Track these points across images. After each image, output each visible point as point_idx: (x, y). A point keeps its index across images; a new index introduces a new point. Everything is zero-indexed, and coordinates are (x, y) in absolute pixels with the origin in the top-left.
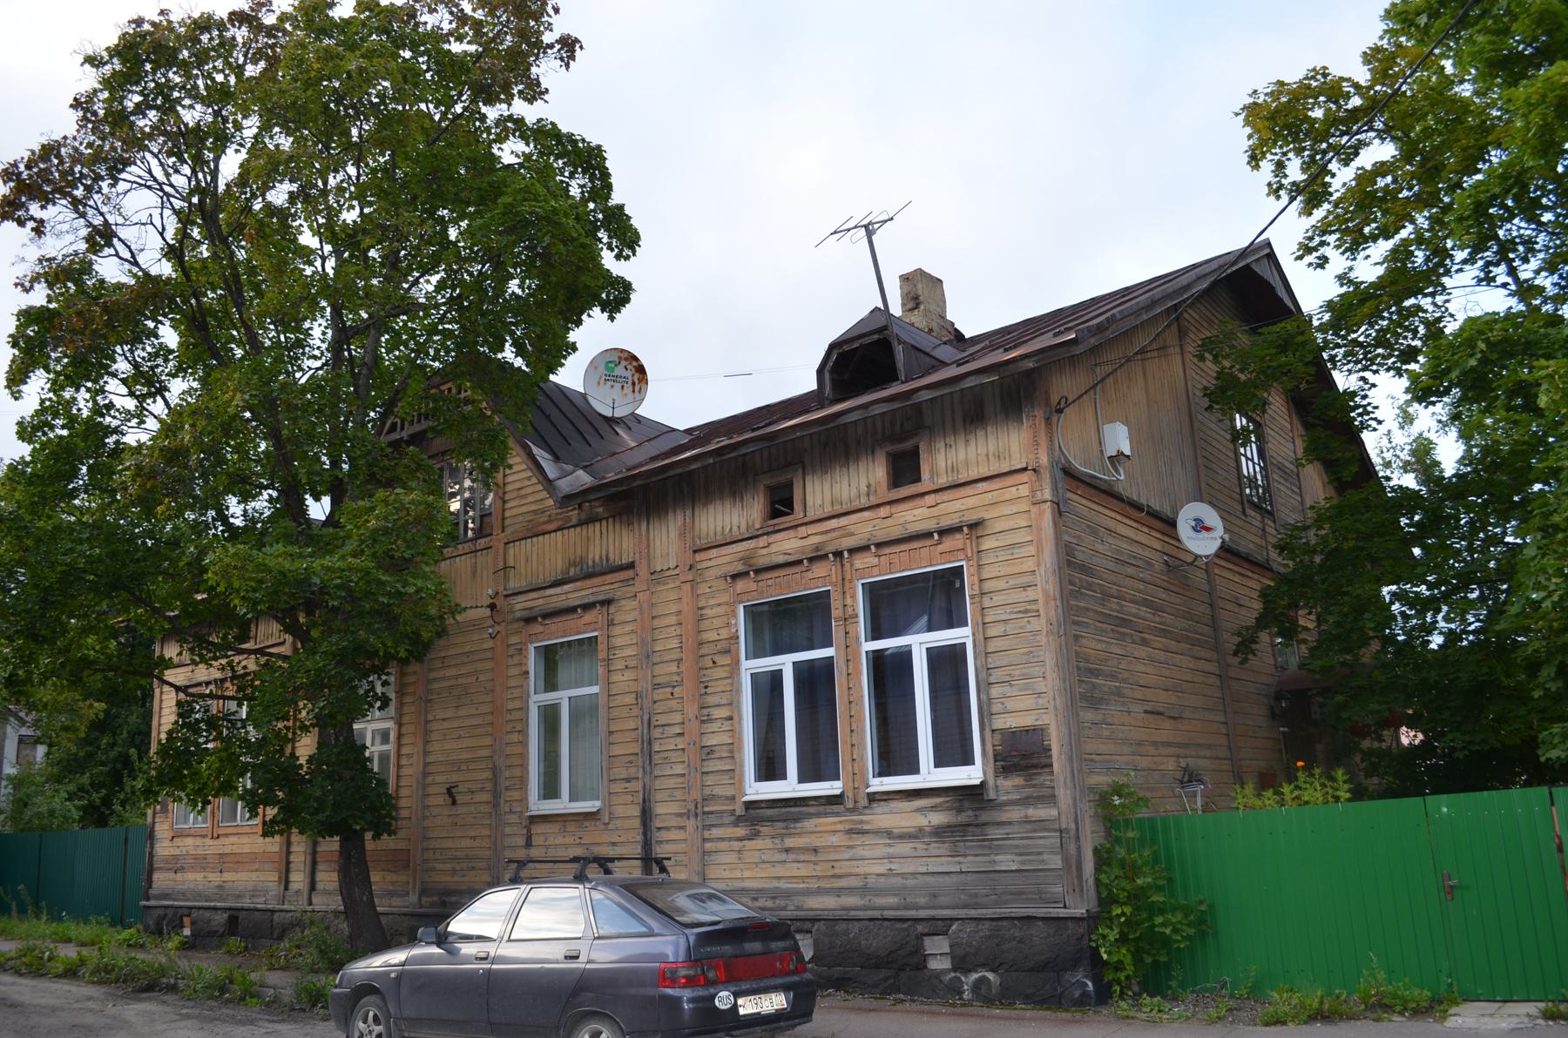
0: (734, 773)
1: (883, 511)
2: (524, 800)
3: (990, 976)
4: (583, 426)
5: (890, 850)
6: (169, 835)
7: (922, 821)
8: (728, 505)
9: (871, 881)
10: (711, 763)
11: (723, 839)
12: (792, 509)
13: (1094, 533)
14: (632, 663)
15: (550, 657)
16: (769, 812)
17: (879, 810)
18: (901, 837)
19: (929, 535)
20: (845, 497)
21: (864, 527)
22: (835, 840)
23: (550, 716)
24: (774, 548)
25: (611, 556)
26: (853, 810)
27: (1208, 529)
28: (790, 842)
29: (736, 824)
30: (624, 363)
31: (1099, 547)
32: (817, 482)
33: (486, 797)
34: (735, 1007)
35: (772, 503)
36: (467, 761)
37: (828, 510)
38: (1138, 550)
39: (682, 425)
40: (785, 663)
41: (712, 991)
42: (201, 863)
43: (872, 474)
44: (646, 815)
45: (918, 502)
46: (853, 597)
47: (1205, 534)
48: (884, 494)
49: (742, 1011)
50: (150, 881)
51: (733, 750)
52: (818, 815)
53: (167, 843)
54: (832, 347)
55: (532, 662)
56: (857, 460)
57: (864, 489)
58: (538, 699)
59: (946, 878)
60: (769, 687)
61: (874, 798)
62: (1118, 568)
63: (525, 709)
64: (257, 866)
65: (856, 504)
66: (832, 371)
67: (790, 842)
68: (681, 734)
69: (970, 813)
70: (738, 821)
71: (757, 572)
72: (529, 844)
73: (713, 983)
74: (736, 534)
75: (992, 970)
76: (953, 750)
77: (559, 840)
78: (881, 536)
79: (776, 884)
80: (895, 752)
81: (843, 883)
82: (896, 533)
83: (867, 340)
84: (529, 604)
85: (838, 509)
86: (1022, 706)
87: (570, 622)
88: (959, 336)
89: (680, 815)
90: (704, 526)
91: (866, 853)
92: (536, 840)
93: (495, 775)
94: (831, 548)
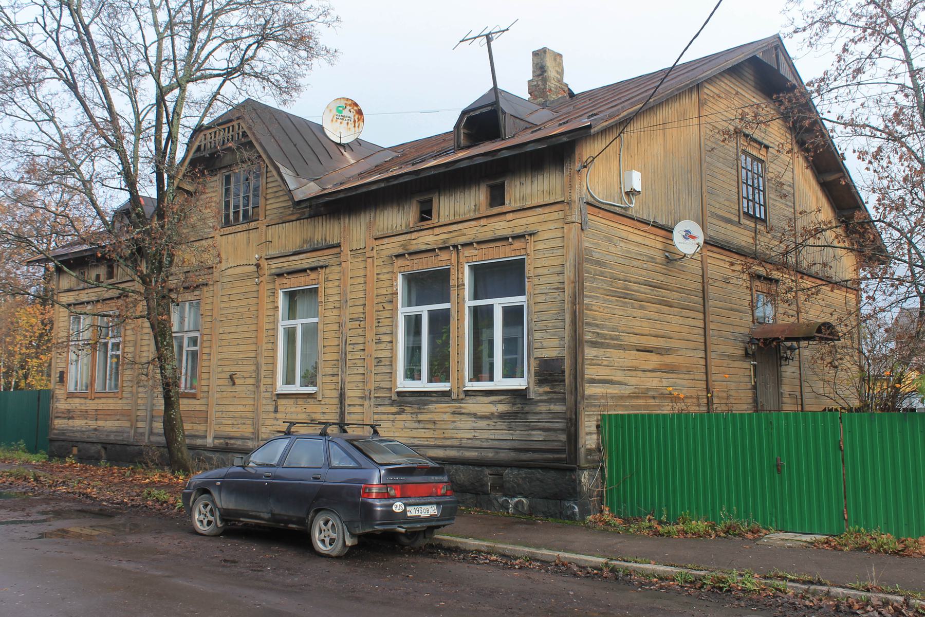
0: (391, 374)
1: (483, 222)
2: (273, 384)
3: (524, 500)
4: (319, 150)
5: (475, 425)
6: (65, 396)
7: (493, 409)
8: (395, 210)
9: (464, 441)
10: (380, 368)
11: (384, 413)
12: (431, 216)
13: (610, 240)
14: (337, 305)
15: (292, 296)
16: (410, 399)
17: (470, 401)
18: (483, 417)
19: (506, 239)
20: (462, 211)
21: (471, 232)
22: (447, 417)
23: (290, 334)
24: (420, 240)
25: (328, 238)
26: (458, 400)
27: (694, 237)
28: (421, 417)
29: (392, 405)
30: (348, 108)
31: (613, 249)
32: (446, 200)
33: (252, 381)
34: (405, 511)
35: (422, 212)
36: (242, 359)
37: (452, 219)
38: (644, 250)
39: (386, 145)
40: (424, 311)
41: (391, 501)
42: (85, 414)
43: (478, 197)
44: (342, 397)
45: (502, 218)
46: (463, 273)
47: (691, 240)
48: (484, 210)
49: (409, 514)
50: (922, 303)
51: (392, 361)
52: (437, 402)
53: (63, 402)
54: (464, 113)
55: (281, 301)
56: (470, 188)
57: (473, 207)
58: (283, 324)
59: (505, 442)
60: (414, 324)
61: (468, 393)
62: (626, 262)
63: (275, 329)
64: (118, 417)
65: (468, 217)
66: (465, 127)
67: (421, 417)
68: (364, 350)
69: (519, 406)
70: (393, 402)
71: (410, 254)
72: (276, 411)
73: (393, 497)
74: (399, 230)
75: (526, 497)
76: (511, 370)
77: (293, 409)
78: (481, 237)
79: (412, 441)
80: (480, 370)
81: (448, 442)
82: (489, 236)
83: (484, 110)
84: (280, 265)
85: (458, 219)
86: (551, 345)
87: (102, 358)
88: (571, 95)
89: (362, 398)
90: (381, 224)
91: (462, 425)
92: (280, 408)
93: (257, 368)
94: (452, 242)
